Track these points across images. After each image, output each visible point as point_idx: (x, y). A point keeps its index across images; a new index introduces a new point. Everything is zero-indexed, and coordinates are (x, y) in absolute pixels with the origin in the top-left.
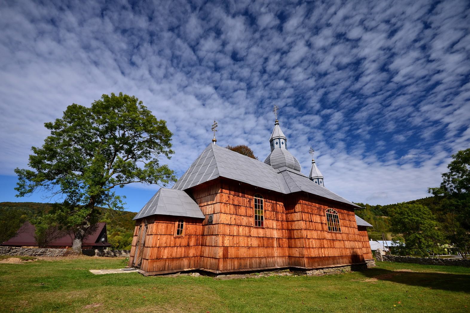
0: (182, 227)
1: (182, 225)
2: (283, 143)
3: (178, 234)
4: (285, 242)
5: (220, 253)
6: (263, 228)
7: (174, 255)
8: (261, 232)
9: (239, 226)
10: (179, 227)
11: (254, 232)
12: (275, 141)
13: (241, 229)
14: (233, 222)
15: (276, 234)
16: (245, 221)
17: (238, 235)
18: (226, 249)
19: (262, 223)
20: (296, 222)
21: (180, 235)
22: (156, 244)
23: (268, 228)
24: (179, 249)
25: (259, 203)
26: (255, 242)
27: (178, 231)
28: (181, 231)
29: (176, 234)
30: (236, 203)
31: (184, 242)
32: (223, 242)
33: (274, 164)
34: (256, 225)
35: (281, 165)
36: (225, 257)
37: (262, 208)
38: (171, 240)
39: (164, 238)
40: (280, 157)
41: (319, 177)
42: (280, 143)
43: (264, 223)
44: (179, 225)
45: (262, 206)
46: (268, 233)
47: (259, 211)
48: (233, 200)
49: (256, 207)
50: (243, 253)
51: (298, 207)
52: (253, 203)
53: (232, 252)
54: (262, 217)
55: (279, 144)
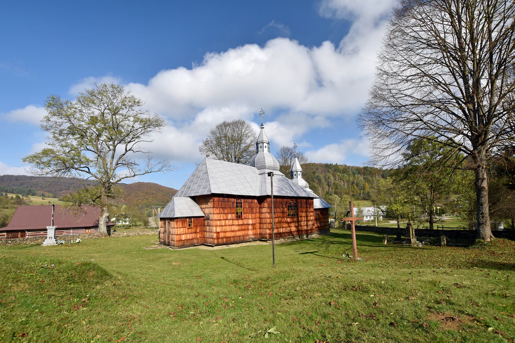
0: (191, 223)
1: (191, 221)
2: (266, 147)
3: (189, 226)
4: (258, 226)
5: (215, 236)
6: (242, 219)
7: (188, 238)
8: (240, 222)
9: (226, 220)
10: (189, 223)
11: (236, 222)
12: (259, 145)
13: (227, 221)
14: (222, 218)
15: (250, 222)
16: (230, 216)
17: (226, 225)
18: (218, 233)
19: (241, 216)
20: (264, 214)
21: (190, 227)
22: (178, 233)
23: (245, 218)
24: (191, 235)
25: (239, 204)
26: (236, 228)
27: (189, 224)
28: (191, 224)
29: (188, 227)
30: (223, 206)
31: (193, 230)
32: (216, 230)
33: (258, 166)
34: (237, 218)
35: (262, 167)
36: (218, 238)
37: (241, 207)
38: (186, 230)
39: (182, 229)
40: (262, 160)
41: (298, 171)
42: (263, 147)
43: (243, 216)
44: (189, 221)
45: (241, 206)
46: (245, 222)
47: (239, 209)
48: (221, 205)
49: (237, 207)
50: (228, 234)
52: (235, 205)
53: (222, 235)
54: (241, 213)
55: (262, 148)
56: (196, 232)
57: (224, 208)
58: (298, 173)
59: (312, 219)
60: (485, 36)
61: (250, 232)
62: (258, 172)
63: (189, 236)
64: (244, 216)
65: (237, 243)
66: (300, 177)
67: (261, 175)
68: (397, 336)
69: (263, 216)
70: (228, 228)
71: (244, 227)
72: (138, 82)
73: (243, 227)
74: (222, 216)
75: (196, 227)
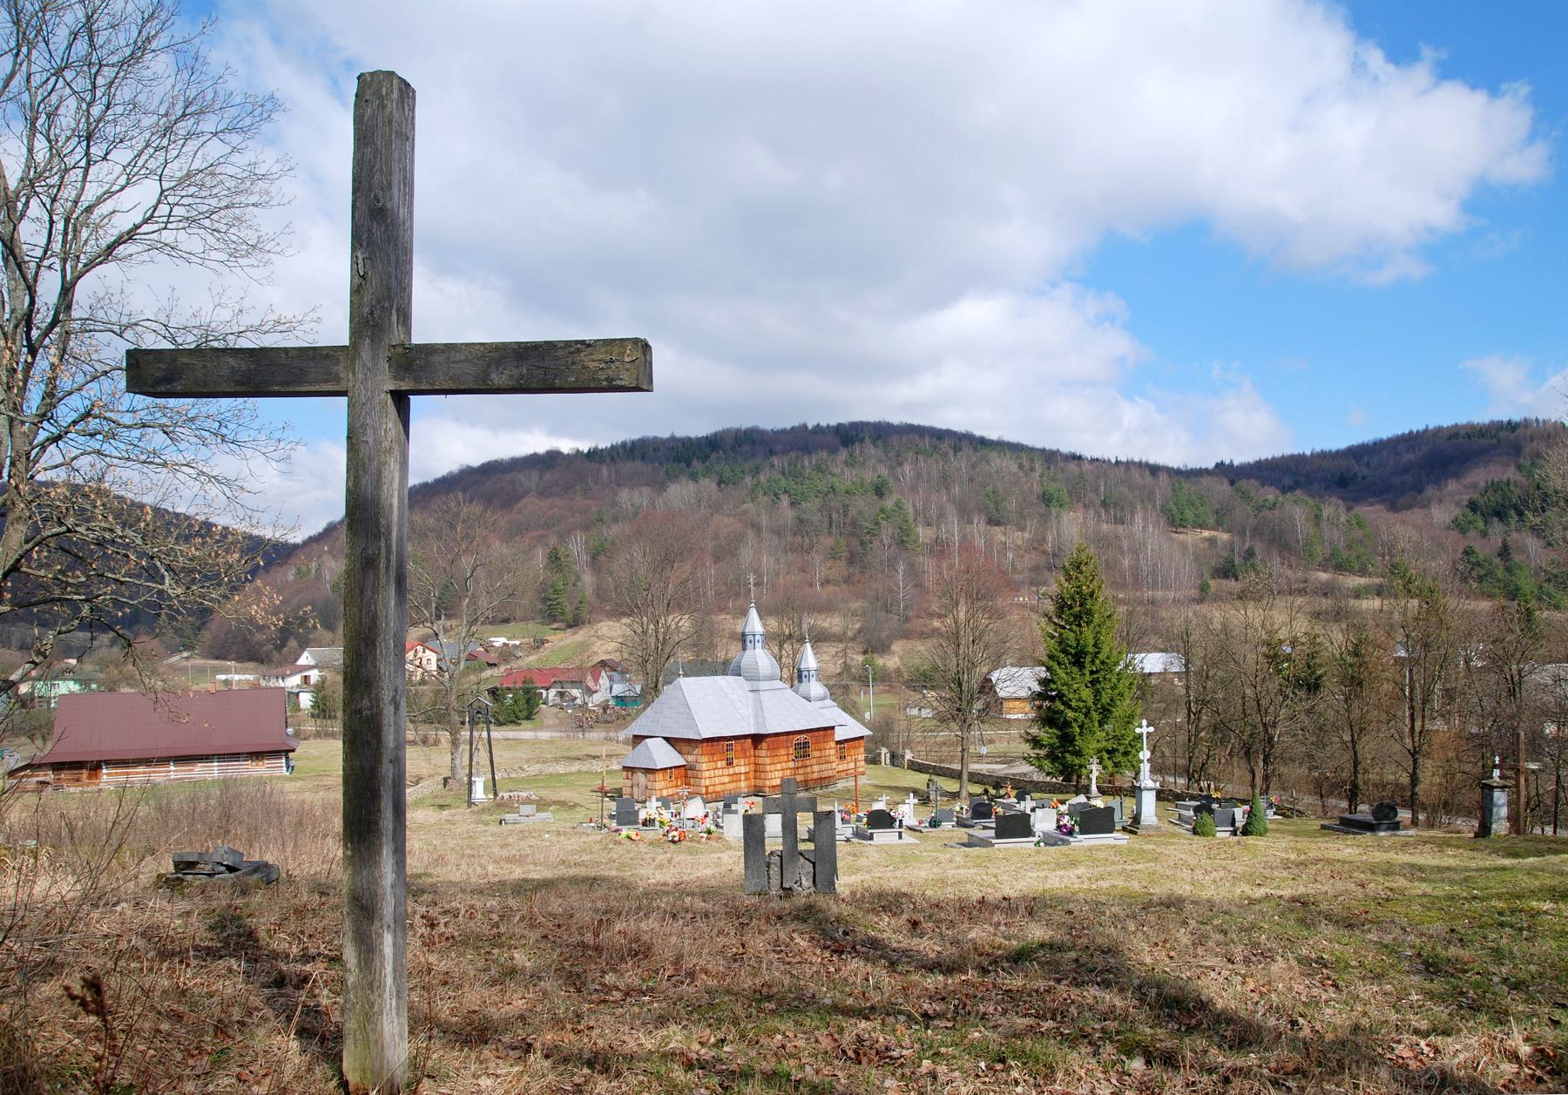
5: (704, 790)
8: (731, 771)
11: (726, 772)
15: (743, 770)
18: (707, 787)
26: (726, 779)
31: (674, 783)
46: (737, 770)
50: (718, 788)
51: (764, 745)
56: (677, 786)
57: (712, 754)
58: (757, 637)
59: (604, 681)
60: (1412, 836)
61: (743, 784)
62: (747, 685)
63: (671, 791)
64: (735, 762)
65: (516, 740)
66: (759, 645)
67: (752, 694)
68: (1432, 980)
69: (760, 761)
70: (717, 780)
71: (735, 778)
72: (897, 426)
73: (735, 778)
74: (712, 765)
75: (677, 779)
